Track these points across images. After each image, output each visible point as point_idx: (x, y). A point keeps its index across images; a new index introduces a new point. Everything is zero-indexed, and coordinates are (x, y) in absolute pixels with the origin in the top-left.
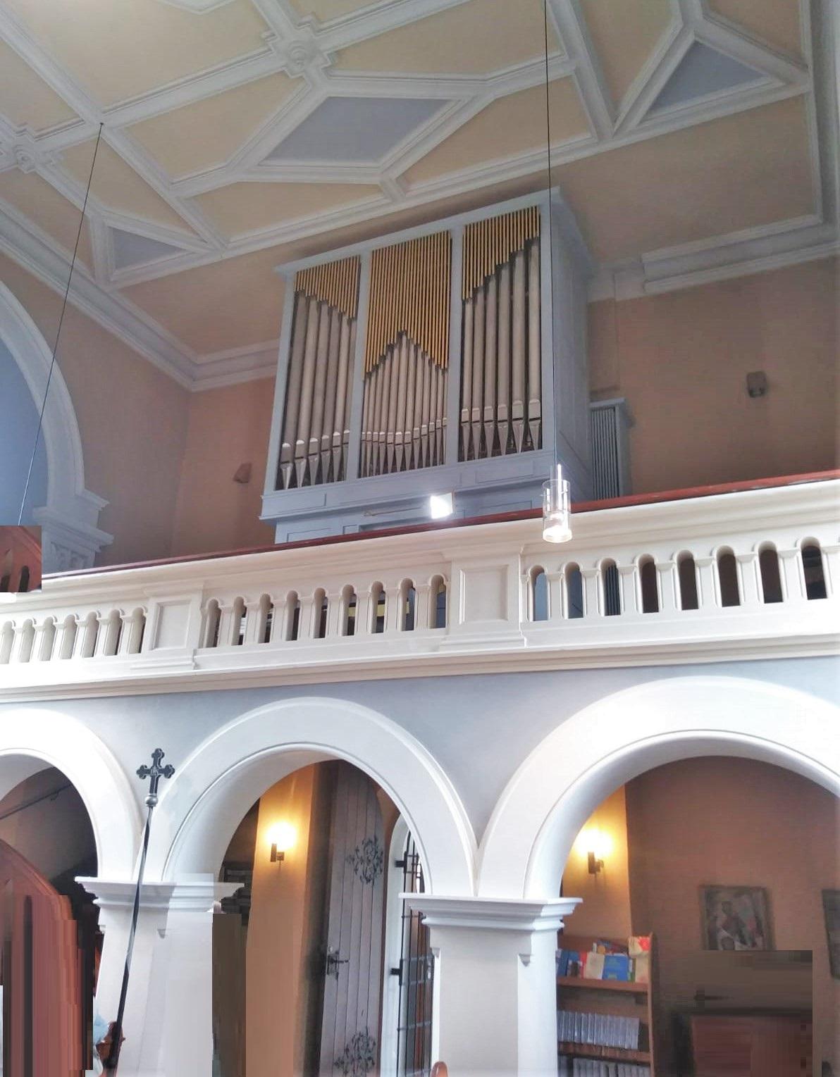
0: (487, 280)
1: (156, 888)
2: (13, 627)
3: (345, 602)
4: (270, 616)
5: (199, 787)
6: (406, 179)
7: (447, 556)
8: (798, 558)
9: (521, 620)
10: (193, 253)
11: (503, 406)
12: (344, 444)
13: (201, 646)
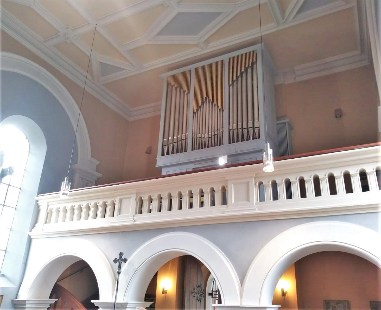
0: (237, 78)
1: (121, 304)
2: (74, 208)
3: (200, 195)
4: (161, 202)
5: (136, 266)
6: (207, 42)
7: (227, 178)
8: (374, 174)
9: (255, 201)
10: (130, 70)
11: (245, 123)
12: (186, 138)
13: (136, 214)
